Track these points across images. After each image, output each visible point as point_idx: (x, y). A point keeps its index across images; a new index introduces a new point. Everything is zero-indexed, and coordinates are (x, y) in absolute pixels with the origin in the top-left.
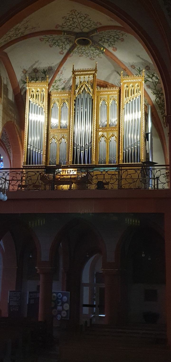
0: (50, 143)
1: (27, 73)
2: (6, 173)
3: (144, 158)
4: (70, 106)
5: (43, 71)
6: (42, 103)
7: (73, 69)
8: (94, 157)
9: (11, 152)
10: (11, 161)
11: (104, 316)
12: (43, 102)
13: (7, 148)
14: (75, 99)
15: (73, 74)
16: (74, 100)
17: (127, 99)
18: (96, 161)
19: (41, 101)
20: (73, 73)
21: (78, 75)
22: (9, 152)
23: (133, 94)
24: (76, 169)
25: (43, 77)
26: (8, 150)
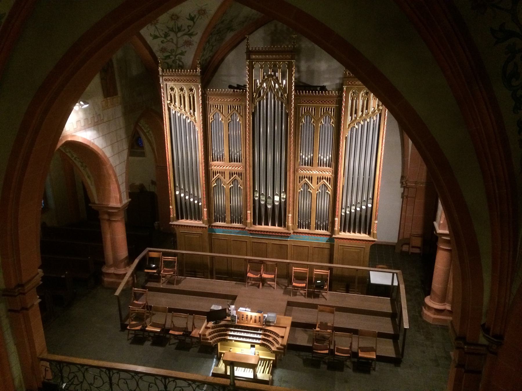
0: (213, 186)
1: (158, 22)
2: (137, 375)
3: (371, 197)
4: (246, 151)
5: (188, 17)
6: (192, 114)
7: (248, 48)
8: (280, 107)
9: (152, 137)
10: (155, 150)
11: (273, 81)
12: (194, 111)
13: (145, 131)
14: (253, 111)
15: (247, 59)
16: (251, 113)
17: (353, 119)
18: (293, 224)
19: (190, 109)
20: (248, 58)
21: (258, 60)
22: (149, 137)
23: (367, 109)
24: (250, 56)
25: (190, 26)
26: (147, 134)
